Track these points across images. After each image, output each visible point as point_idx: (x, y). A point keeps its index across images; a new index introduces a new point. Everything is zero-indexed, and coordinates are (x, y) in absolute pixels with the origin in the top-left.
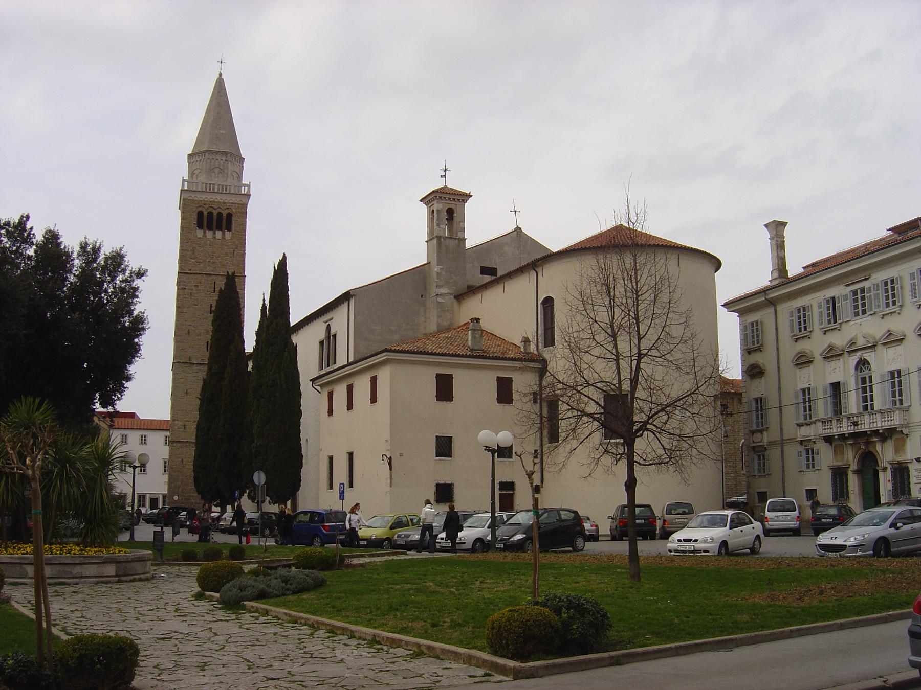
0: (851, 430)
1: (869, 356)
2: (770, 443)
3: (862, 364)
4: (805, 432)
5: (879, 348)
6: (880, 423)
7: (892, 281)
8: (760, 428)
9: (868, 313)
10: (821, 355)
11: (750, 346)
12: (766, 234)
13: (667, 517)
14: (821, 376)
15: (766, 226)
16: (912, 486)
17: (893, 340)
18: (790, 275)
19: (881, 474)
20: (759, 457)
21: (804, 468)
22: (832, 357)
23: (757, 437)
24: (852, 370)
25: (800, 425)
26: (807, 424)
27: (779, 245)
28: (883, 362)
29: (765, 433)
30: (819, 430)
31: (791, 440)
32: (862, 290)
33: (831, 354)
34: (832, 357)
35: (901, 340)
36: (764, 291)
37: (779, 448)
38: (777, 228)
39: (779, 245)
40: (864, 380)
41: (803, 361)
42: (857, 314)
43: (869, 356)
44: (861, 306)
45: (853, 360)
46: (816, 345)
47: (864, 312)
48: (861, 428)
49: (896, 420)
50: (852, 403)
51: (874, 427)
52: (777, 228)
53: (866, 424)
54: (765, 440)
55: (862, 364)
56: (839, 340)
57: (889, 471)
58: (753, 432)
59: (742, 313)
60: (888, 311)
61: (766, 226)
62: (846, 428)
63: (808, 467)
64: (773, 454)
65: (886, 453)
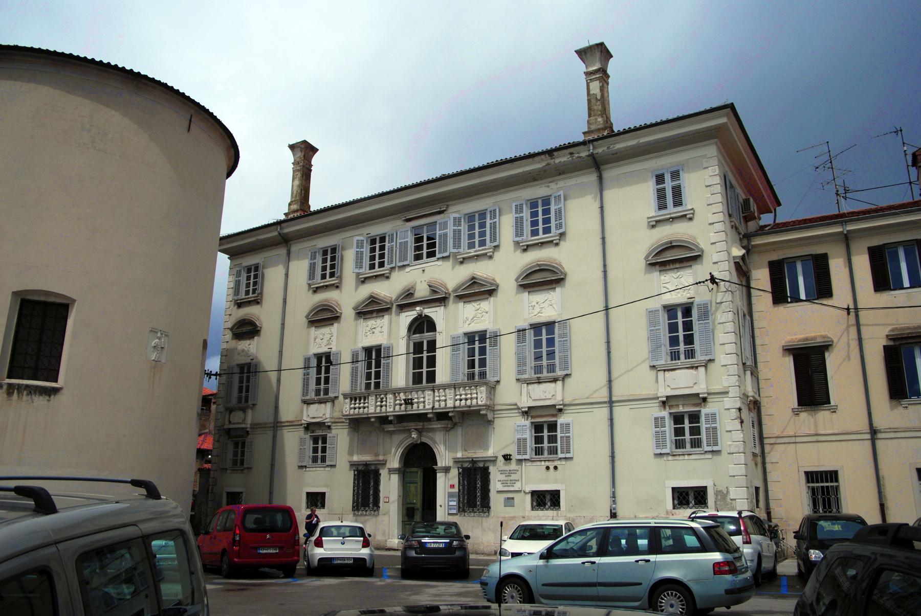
0: (401, 410)
1: (436, 313)
2: (255, 426)
3: (422, 325)
4: (319, 412)
5: (451, 305)
6: (449, 401)
7: (383, 239)
8: (243, 404)
9: (438, 256)
10: (355, 309)
11: (242, 295)
12: (289, 158)
13: (341, 397)
14: (348, 338)
15: (292, 147)
16: (493, 494)
17: (478, 291)
18: (312, 209)
19: (441, 479)
20: (236, 445)
21: (308, 462)
22: (371, 312)
23: (237, 417)
24: (404, 331)
25: (308, 403)
26: (320, 402)
27: (304, 172)
28: (454, 322)
29: (250, 412)
30: (347, 408)
31: (292, 424)
32: (482, 215)
33: (372, 309)
34: (371, 312)
35: (491, 293)
36: (279, 223)
37: (270, 433)
38: (305, 152)
39: (304, 172)
40: (418, 348)
41: (324, 316)
42: (418, 257)
43: (436, 313)
44: (426, 248)
45: (408, 317)
46: (348, 297)
47: (431, 255)
48: (415, 409)
49: (480, 397)
50: (399, 372)
51: (440, 406)
52: (305, 152)
53: (426, 402)
54: (249, 420)
55: (422, 325)
56: (387, 290)
57: (454, 472)
58: (231, 410)
59: (233, 254)
60: (472, 252)
61: (292, 147)
62: (392, 407)
63: (315, 460)
64: (260, 444)
65: (447, 454)
